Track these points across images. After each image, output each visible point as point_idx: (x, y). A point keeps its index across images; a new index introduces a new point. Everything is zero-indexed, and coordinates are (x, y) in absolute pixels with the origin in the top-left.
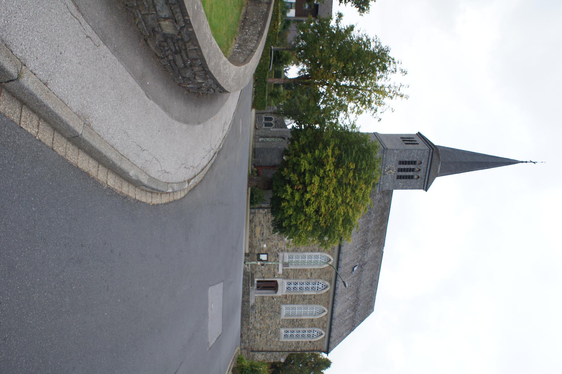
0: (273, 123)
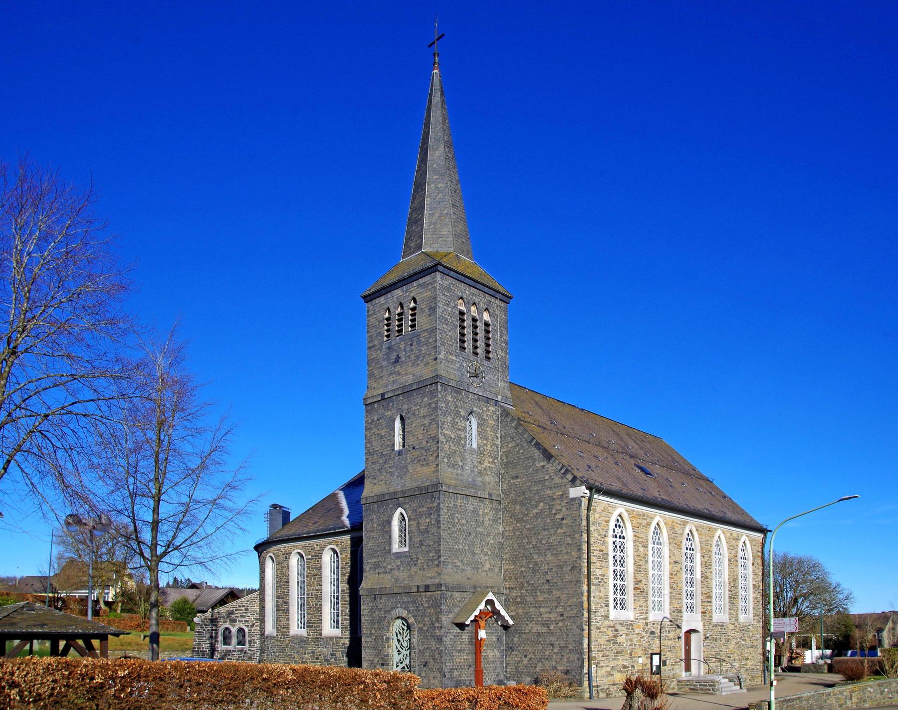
0: (236, 628)
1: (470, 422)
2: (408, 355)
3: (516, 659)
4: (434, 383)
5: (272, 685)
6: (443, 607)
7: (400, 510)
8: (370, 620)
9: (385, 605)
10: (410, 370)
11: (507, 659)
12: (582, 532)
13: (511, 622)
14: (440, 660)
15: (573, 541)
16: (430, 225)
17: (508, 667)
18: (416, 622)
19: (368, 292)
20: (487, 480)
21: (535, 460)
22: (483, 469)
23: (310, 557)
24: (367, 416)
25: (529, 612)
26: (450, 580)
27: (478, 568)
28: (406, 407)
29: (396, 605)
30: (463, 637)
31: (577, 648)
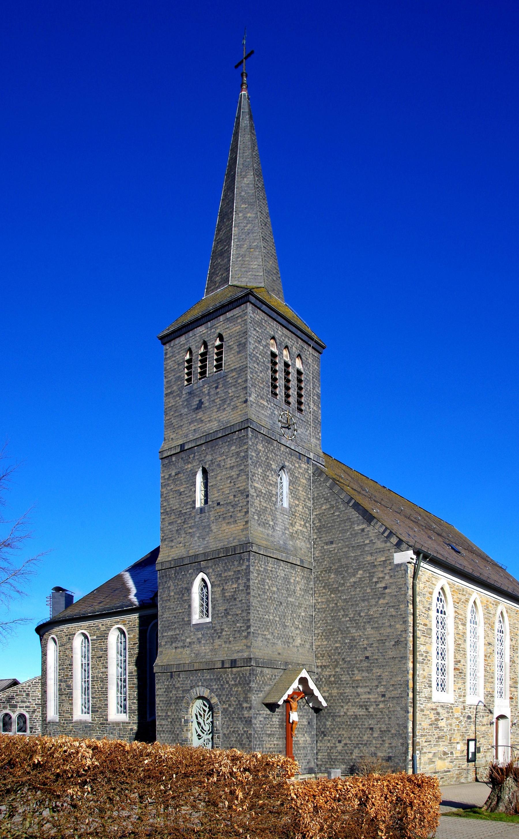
0: (17, 713)
1: (281, 479)
2: (212, 399)
3: (329, 744)
4: (243, 429)
5: (53, 777)
6: (253, 685)
7: (201, 575)
8: (166, 701)
9: (183, 684)
10: (214, 416)
11: (318, 745)
12: (408, 602)
13: (324, 704)
14: (249, 745)
15: (397, 612)
16: (238, 257)
17: (319, 754)
18: (220, 702)
19: (166, 332)
20: (299, 545)
21: (353, 523)
22: (294, 532)
23: (95, 637)
24: (163, 471)
25: (345, 693)
26: (261, 654)
27: (289, 643)
28: (209, 457)
29: (196, 683)
30: (274, 720)
31: (401, 732)
